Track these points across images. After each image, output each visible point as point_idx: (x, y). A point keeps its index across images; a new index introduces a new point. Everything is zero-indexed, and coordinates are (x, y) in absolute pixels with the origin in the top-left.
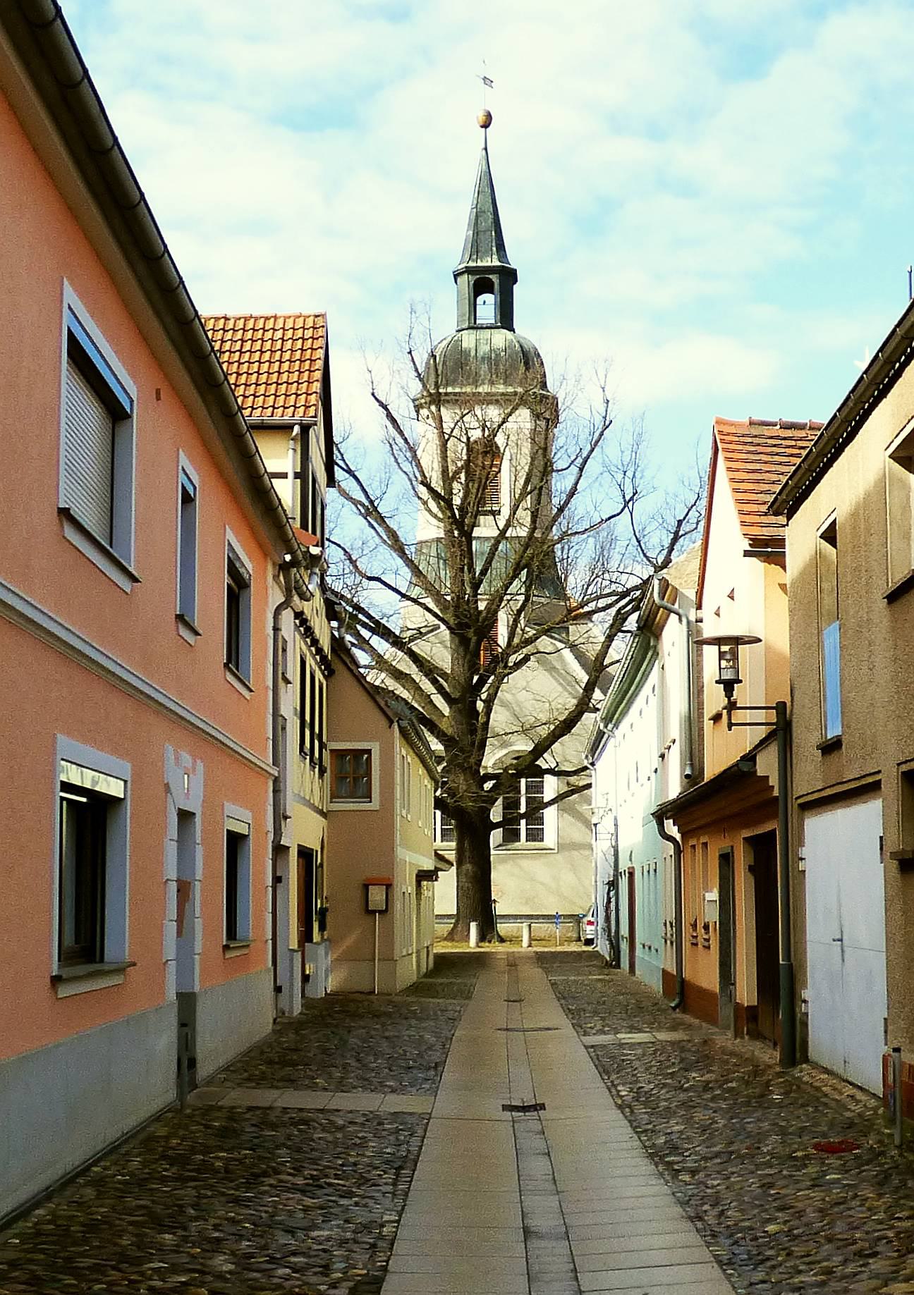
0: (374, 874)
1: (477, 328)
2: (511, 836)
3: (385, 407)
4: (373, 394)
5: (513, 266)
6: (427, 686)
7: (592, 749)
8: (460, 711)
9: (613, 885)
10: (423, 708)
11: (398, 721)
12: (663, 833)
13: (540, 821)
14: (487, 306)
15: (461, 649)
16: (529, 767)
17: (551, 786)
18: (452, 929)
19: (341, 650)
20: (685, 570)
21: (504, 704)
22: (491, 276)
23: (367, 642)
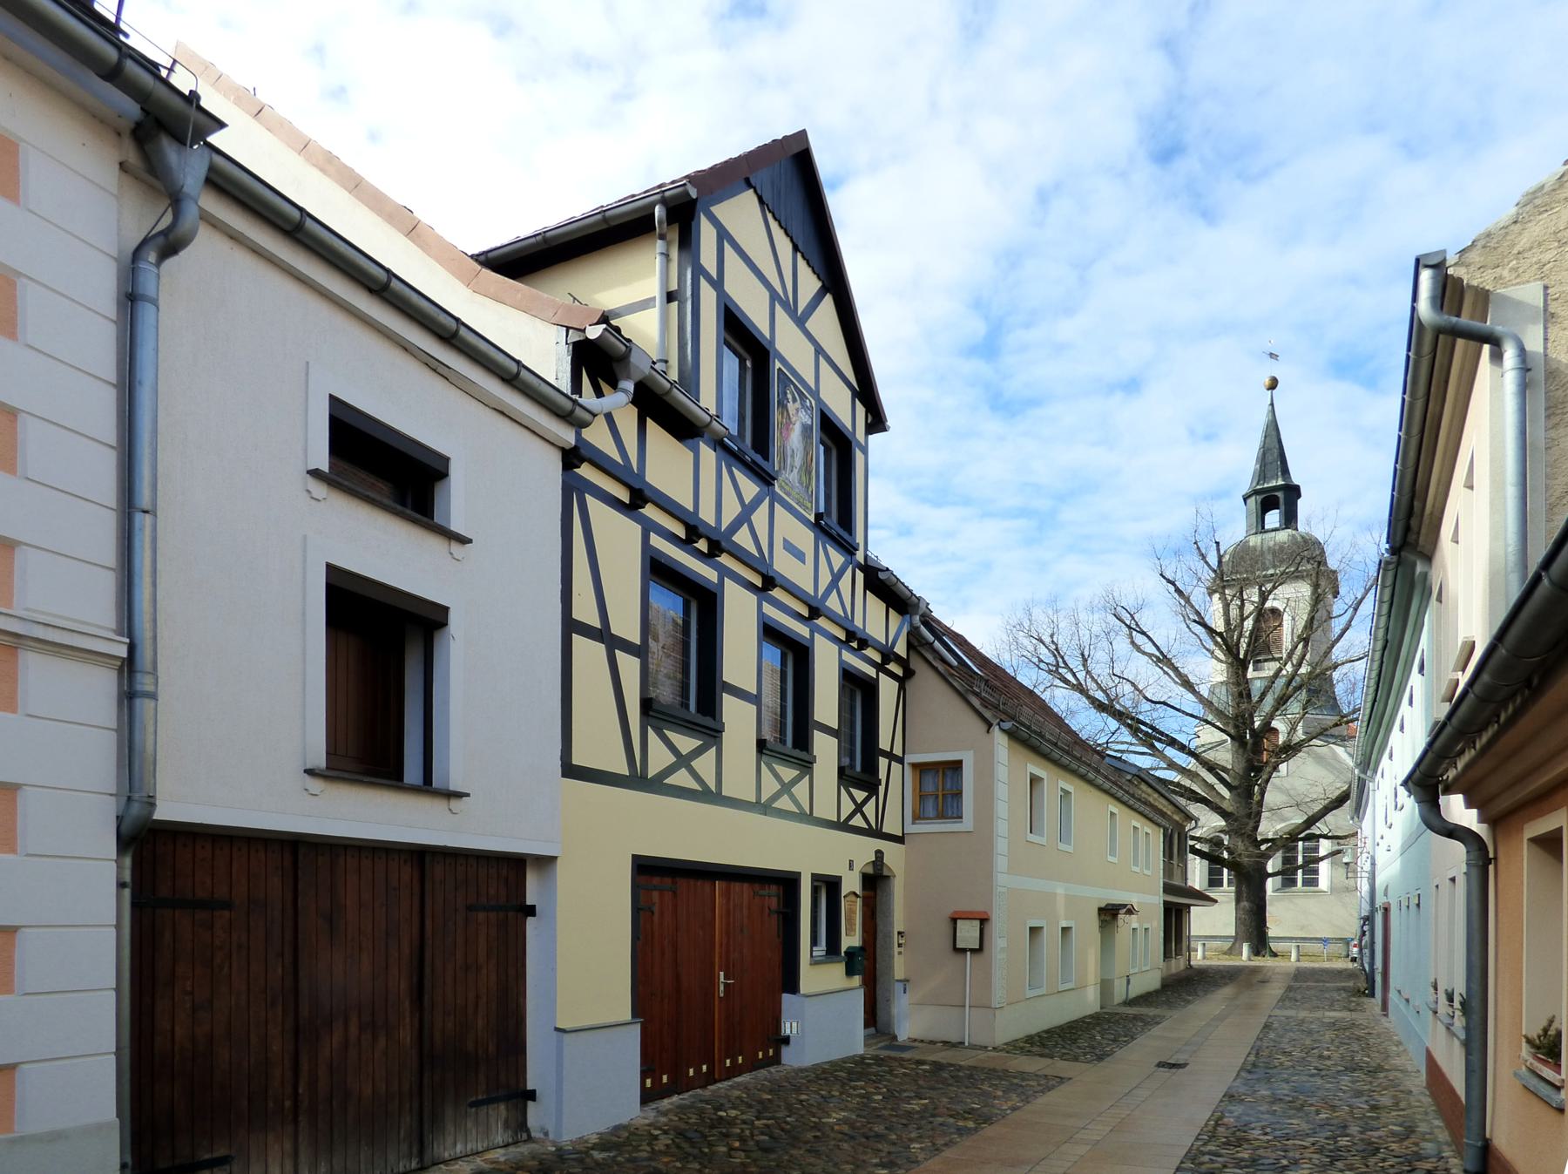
0: (965, 906)
1: (1265, 532)
2: (1289, 882)
3: (1173, 583)
4: (1161, 575)
5: (1296, 483)
6: (1211, 779)
7: (1356, 809)
8: (1239, 795)
9: (1368, 920)
10: (1207, 794)
11: (999, 724)
12: (1436, 822)
13: (1316, 872)
14: (1273, 518)
15: (1241, 751)
16: (1305, 833)
17: (1325, 847)
18: (1231, 947)
19: (920, 646)
20: (1513, 245)
21: (1279, 789)
22: (1276, 494)
23: (1161, 752)
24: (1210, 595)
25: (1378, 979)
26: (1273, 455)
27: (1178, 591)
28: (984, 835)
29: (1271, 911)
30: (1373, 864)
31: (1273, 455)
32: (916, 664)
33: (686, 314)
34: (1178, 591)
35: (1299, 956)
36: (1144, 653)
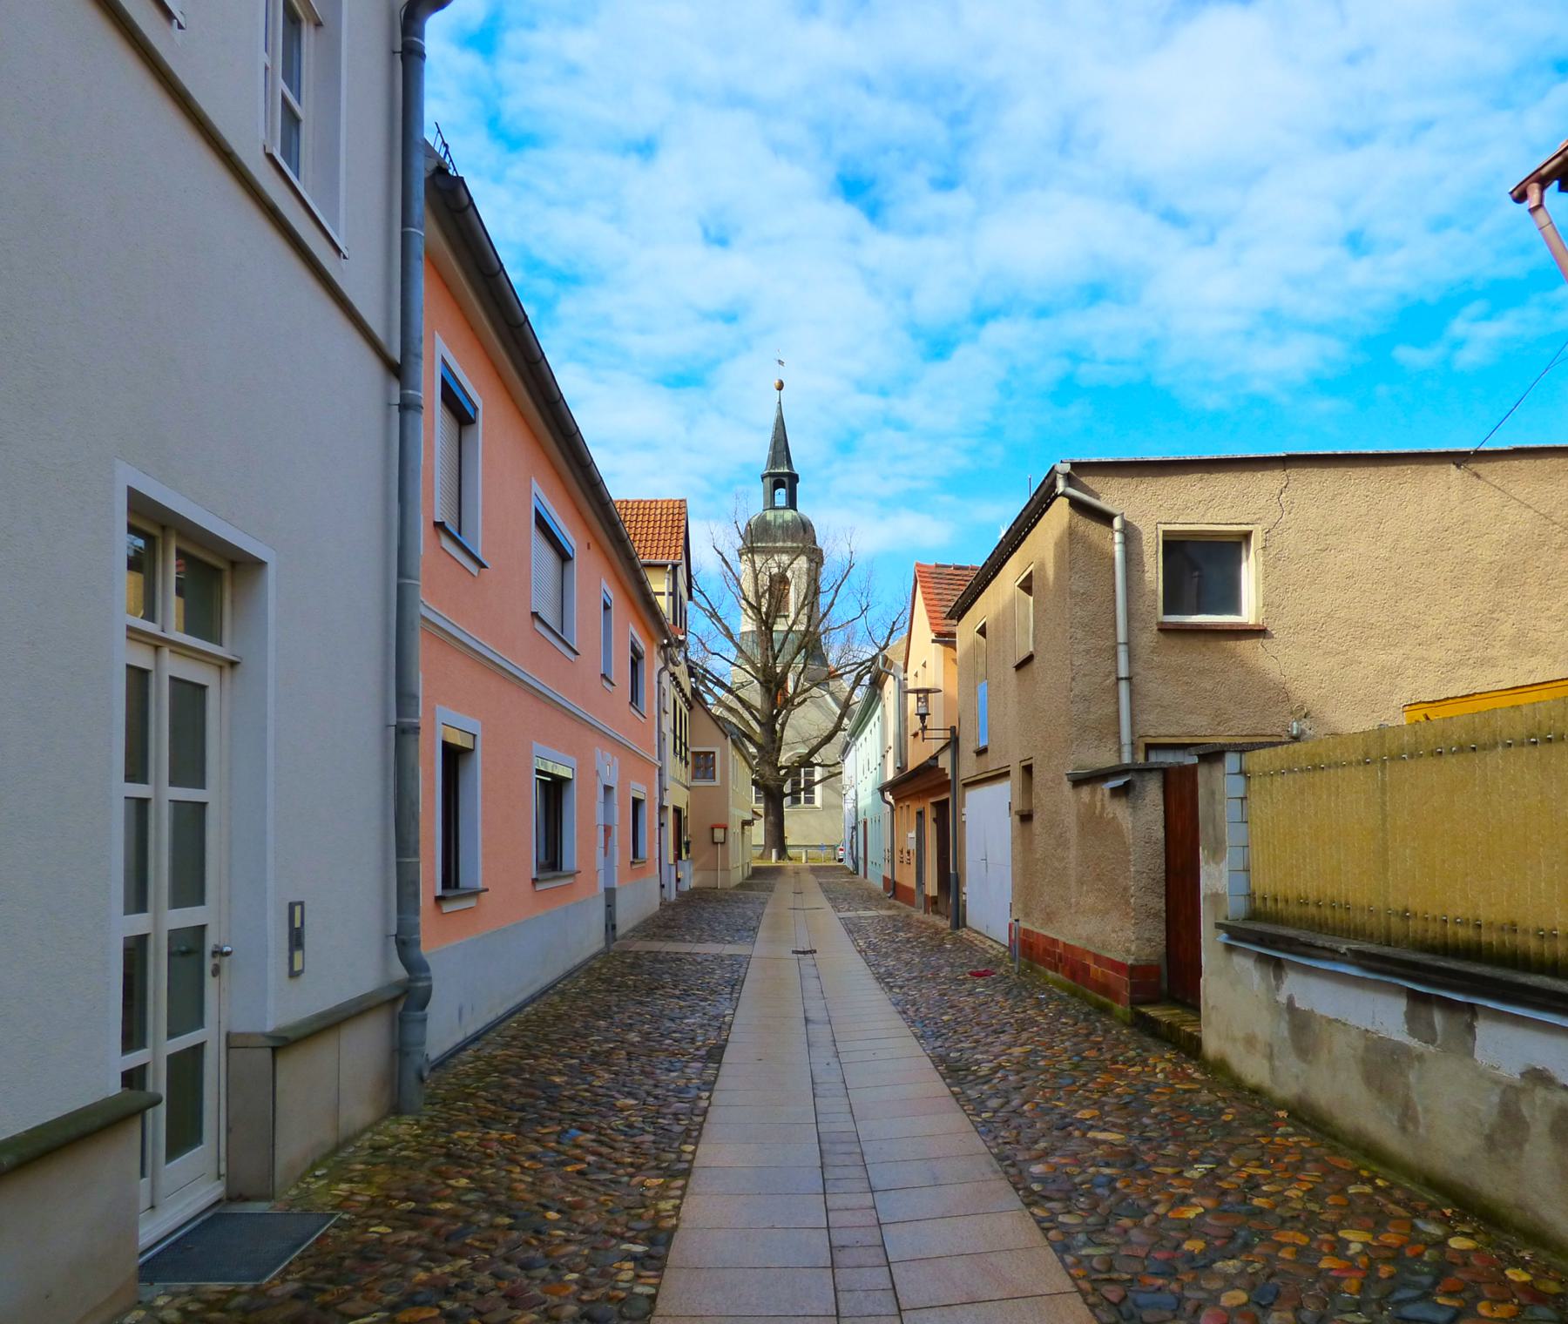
2: (796, 801)
3: (721, 554)
6: (746, 715)
8: (766, 731)
9: (855, 828)
13: (813, 792)
14: (781, 496)
16: (806, 762)
24: (740, 556)
25: (861, 863)
26: (780, 448)
27: (724, 559)
28: (724, 790)
29: (788, 823)
30: (856, 795)
31: (780, 448)
32: (696, 705)
33: (469, 376)
34: (724, 559)
35: (807, 859)
36: (701, 607)
